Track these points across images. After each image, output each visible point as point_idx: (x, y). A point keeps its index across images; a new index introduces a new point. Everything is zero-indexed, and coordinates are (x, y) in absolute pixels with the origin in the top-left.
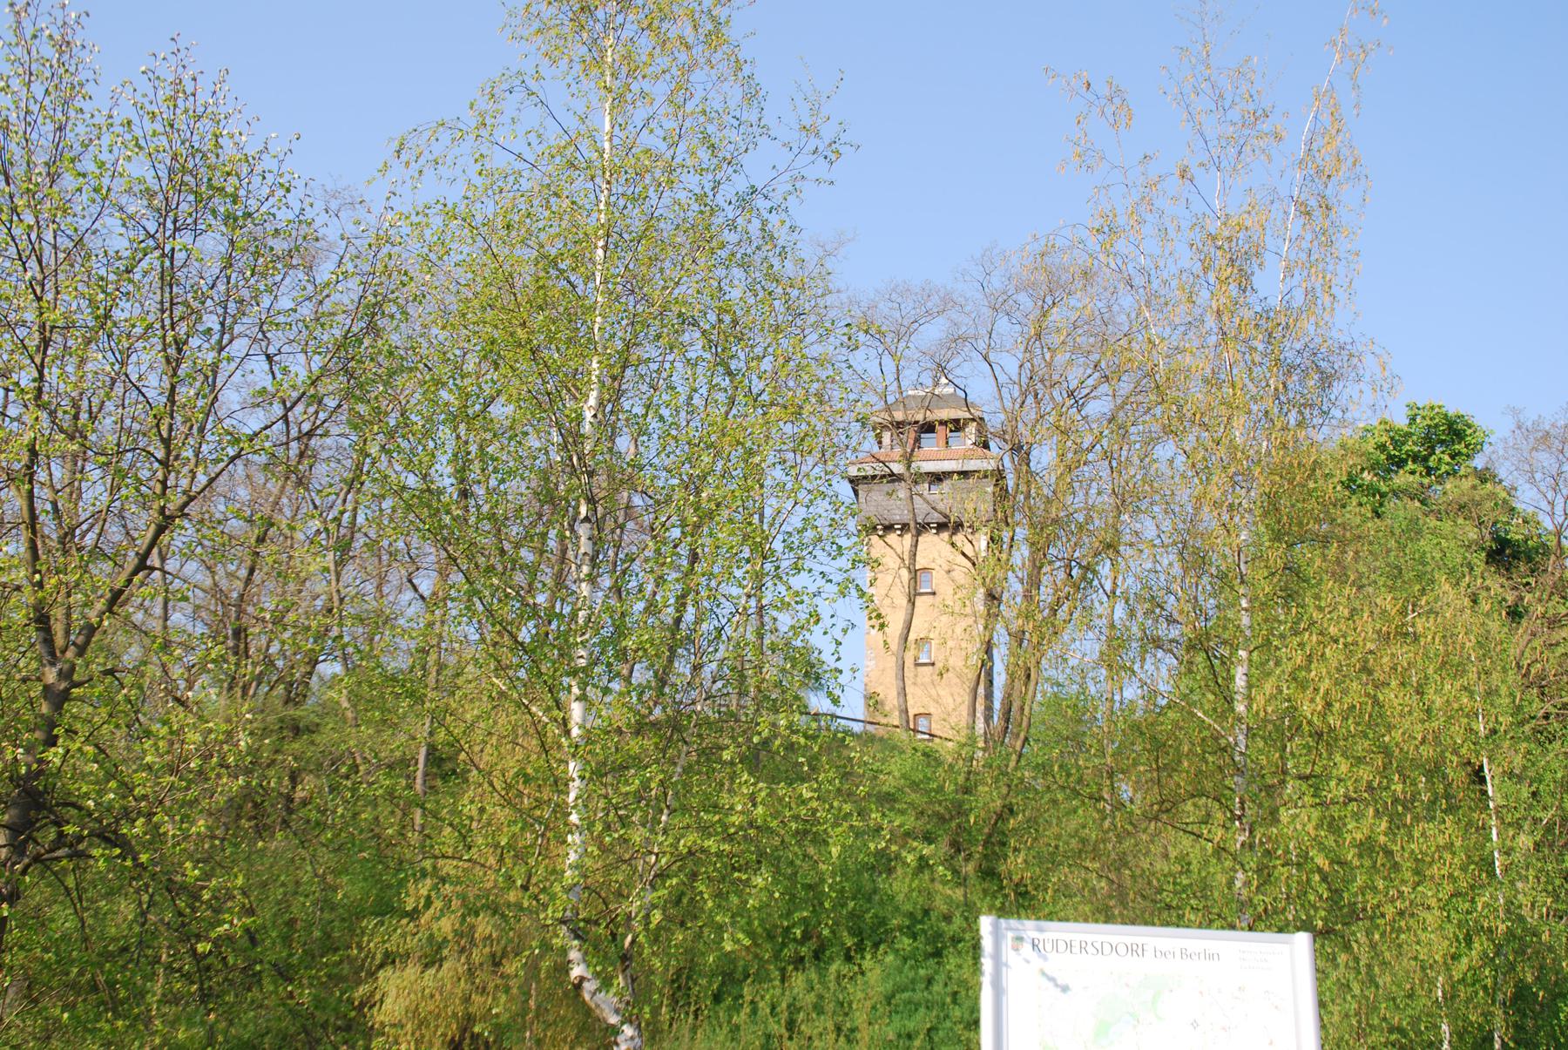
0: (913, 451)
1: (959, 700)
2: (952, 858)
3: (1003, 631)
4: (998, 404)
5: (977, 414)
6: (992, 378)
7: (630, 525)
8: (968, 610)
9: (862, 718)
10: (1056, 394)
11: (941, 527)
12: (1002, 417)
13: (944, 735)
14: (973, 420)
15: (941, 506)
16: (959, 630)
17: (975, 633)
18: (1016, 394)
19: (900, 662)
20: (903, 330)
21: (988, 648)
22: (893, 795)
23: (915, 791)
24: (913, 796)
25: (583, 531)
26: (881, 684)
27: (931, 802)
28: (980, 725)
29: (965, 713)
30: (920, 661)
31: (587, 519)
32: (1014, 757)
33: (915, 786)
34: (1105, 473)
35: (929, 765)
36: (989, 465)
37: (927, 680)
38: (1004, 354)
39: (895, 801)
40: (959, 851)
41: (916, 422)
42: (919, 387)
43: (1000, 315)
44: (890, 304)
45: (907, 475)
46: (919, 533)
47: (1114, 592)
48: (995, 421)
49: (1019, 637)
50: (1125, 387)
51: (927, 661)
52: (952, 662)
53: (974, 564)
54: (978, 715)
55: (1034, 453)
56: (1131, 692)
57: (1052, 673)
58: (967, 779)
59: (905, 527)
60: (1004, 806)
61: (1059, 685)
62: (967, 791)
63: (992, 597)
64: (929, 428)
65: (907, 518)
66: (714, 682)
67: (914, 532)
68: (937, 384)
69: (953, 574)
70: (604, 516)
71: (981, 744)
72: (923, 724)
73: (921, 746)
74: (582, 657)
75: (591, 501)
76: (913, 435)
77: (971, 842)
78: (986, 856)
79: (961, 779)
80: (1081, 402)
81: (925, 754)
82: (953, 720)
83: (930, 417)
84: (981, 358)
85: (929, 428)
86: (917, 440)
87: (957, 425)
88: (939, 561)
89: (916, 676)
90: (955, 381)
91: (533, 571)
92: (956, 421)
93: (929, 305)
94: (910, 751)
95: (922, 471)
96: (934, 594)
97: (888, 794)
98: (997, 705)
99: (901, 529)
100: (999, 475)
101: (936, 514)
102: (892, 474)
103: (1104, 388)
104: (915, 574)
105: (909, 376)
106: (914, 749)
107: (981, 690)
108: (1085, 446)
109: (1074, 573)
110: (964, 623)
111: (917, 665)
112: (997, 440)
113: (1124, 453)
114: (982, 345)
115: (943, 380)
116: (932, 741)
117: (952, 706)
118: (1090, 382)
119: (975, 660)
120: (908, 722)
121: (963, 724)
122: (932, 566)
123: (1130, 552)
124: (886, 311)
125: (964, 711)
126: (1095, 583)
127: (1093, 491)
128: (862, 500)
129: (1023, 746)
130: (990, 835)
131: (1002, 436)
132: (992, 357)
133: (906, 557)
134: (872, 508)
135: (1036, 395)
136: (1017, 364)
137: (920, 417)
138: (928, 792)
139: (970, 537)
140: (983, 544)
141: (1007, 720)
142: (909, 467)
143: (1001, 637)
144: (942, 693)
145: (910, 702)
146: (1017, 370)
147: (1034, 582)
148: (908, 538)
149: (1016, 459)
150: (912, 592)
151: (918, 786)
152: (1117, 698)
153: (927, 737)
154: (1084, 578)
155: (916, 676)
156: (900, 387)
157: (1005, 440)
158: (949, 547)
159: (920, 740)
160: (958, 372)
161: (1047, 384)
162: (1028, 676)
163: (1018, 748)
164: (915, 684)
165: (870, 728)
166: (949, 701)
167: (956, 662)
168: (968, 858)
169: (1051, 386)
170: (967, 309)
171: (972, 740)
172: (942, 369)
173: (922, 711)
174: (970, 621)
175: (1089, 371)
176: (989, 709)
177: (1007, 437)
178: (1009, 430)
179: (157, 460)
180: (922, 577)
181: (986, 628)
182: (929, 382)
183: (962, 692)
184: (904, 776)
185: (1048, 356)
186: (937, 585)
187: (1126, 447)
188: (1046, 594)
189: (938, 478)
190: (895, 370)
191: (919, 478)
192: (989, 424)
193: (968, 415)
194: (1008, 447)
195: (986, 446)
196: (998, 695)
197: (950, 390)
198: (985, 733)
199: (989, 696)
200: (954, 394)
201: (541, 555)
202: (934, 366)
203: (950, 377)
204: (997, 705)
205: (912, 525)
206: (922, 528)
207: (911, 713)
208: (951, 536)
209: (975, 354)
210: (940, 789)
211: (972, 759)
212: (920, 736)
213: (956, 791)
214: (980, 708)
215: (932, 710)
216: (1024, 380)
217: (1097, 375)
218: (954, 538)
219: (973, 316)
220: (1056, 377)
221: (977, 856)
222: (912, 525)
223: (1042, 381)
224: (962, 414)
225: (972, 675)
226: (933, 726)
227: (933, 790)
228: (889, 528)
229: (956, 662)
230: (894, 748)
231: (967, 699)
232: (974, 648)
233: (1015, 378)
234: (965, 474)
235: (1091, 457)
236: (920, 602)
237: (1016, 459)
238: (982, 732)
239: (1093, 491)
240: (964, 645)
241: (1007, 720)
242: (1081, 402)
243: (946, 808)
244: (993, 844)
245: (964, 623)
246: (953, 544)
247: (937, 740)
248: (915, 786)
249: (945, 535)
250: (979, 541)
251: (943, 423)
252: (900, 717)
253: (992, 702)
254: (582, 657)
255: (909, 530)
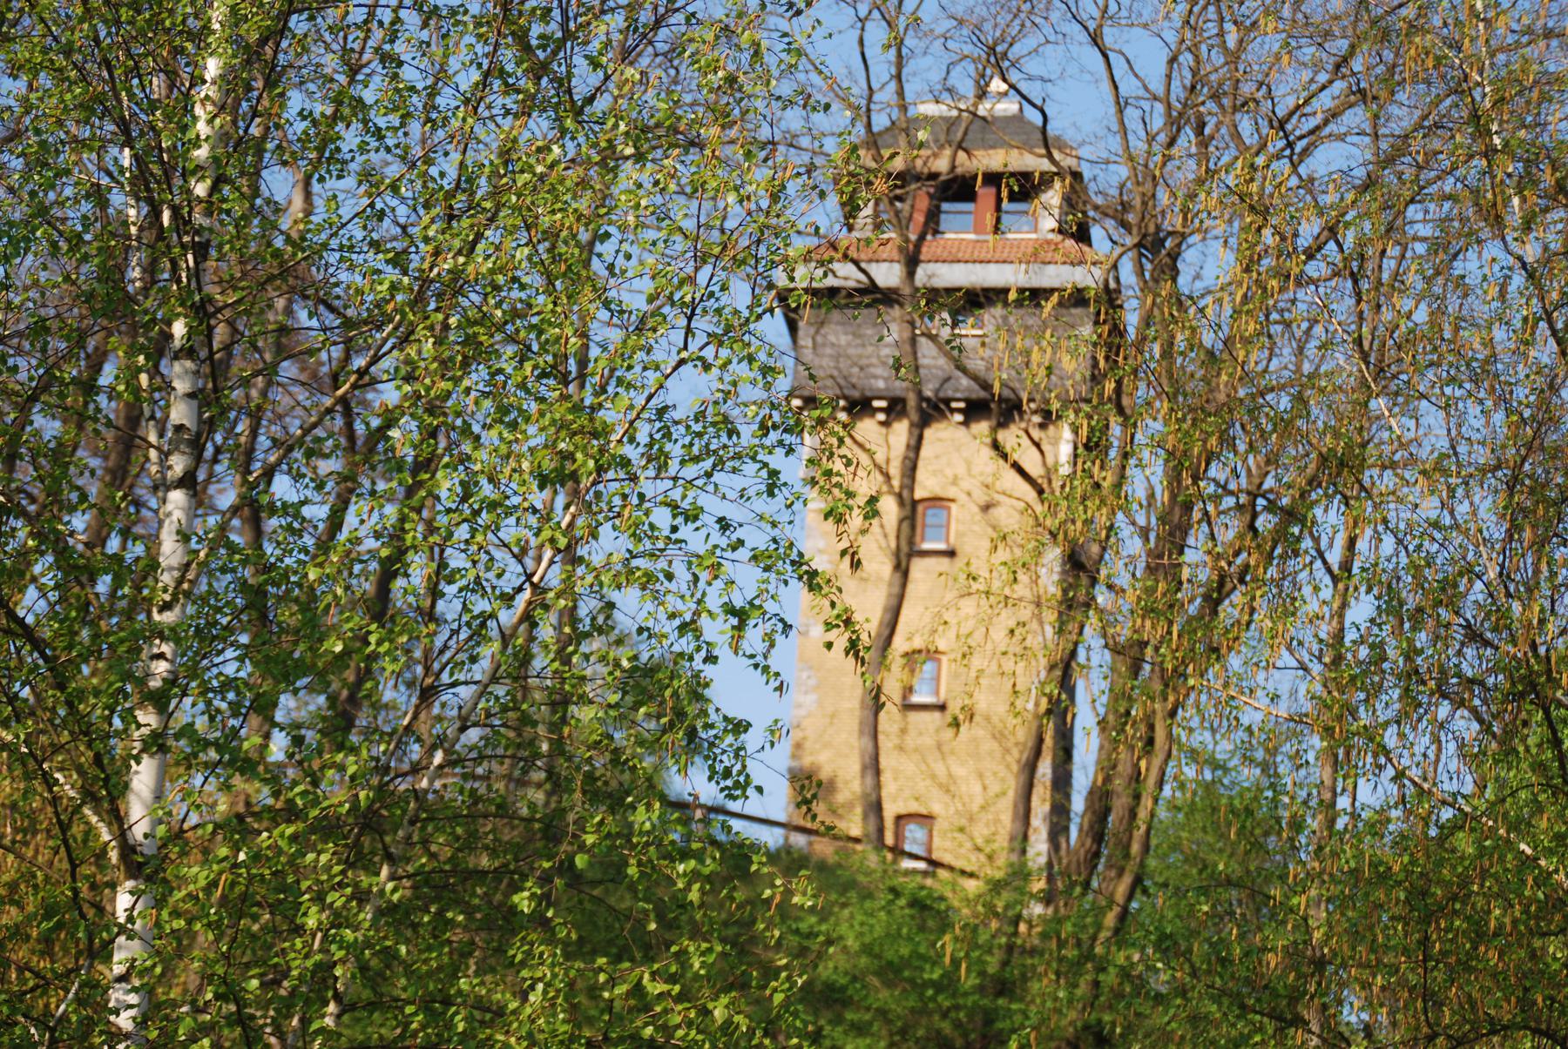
0: (922, 238)
1: (995, 788)
3: (1096, 643)
4: (1115, 143)
5: (1068, 162)
6: (1106, 86)
7: (288, 369)
8: (1022, 590)
9: (782, 818)
10: (1245, 126)
11: (975, 410)
13: (959, 864)
15: (976, 364)
16: (999, 635)
17: (1034, 641)
18: (1157, 122)
19: (894, 602)
21: (1065, 670)
22: (843, 989)
23: (889, 984)
24: (884, 994)
25: (181, 376)
28: (1039, 847)
30: (916, 699)
31: (188, 352)
33: (890, 972)
34: (1344, 306)
35: (922, 928)
36: (1087, 277)
37: (928, 741)
38: (1138, 32)
39: (847, 1003)
41: (933, 176)
42: (945, 96)
46: (924, 421)
47: (1346, 566)
48: (1107, 180)
49: (1130, 655)
50: (1401, 115)
51: (942, 546)
52: (982, 702)
53: (1040, 492)
55: (1190, 258)
56: (1372, 793)
57: (1201, 738)
58: (1005, 964)
59: (896, 408)
60: (1086, 1027)
61: (1216, 765)
62: (1003, 987)
63: (1078, 566)
64: (959, 189)
66: (463, 729)
67: (915, 416)
68: (982, 94)
69: (994, 512)
70: (227, 348)
72: (914, 837)
73: (912, 884)
74: (161, 656)
75: (202, 312)
76: (923, 203)
79: (993, 964)
80: (1299, 147)
81: (915, 903)
82: (980, 832)
84: (1084, 37)
85: (959, 189)
86: (933, 217)
87: (1026, 188)
88: (966, 484)
89: (903, 731)
90: (1023, 87)
91: (61, 454)
92: (1025, 176)
94: (883, 897)
96: (951, 554)
97: (830, 987)
98: (1078, 804)
99: (886, 411)
100: (1111, 297)
101: (965, 382)
102: (872, 288)
103: (1356, 117)
104: (911, 509)
105: (925, 70)
107: (1045, 768)
108: (1304, 242)
109: (1260, 523)
110: (1007, 619)
111: (909, 707)
112: (1110, 223)
113: (1389, 265)
115: (997, 85)
116: (934, 875)
118: (1325, 101)
119: (1032, 704)
120: (881, 830)
121: (1002, 842)
122: (951, 492)
123: (1388, 480)
125: (1005, 814)
126: (1307, 543)
128: (805, 341)
129: (1130, 897)
131: (1119, 213)
132: (1110, 36)
133: (895, 470)
134: (826, 362)
135: (1200, 127)
136: (1164, 55)
137: (941, 165)
139: (1036, 434)
140: (1065, 450)
142: (911, 274)
143: (1095, 656)
144: (959, 771)
146: (1162, 68)
147: (1174, 532)
148: (901, 429)
150: (905, 548)
152: (1343, 802)
153: (922, 865)
154: (1280, 534)
155: (903, 731)
156: (901, 93)
157: (1124, 225)
158: (987, 452)
159: (908, 873)
161: (1226, 101)
162: (1150, 742)
164: (901, 748)
165: (799, 840)
166: (972, 790)
167: (990, 701)
169: (1235, 109)
171: (1020, 874)
172: (996, 59)
173: (914, 807)
174: (1026, 613)
175: (1323, 78)
176: (1060, 811)
177: (1131, 218)
178: (1137, 202)
179: (869, 125)
180: (930, 517)
181: (1060, 632)
182: (967, 88)
183: (1003, 772)
184: (867, 949)
185: (1232, 40)
186: (959, 535)
187: (1394, 251)
188: (1195, 557)
189: (975, 300)
191: (935, 297)
192: (1092, 187)
193: (1045, 165)
194: (1130, 241)
195: (1082, 236)
196: (1083, 777)
197: (1009, 107)
198: (1050, 865)
199: (1062, 781)
200: (1019, 117)
201: (80, 427)
202: (978, 52)
203: (1014, 76)
204: (1078, 804)
206: (932, 410)
208: (994, 430)
210: (948, 984)
211: (1018, 919)
212: (907, 864)
213: (981, 989)
214: (1041, 806)
215: (936, 808)
216: (1177, 90)
217: (1339, 86)
218: (1002, 436)
220: (1247, 89)
223: (1215, 96)
224: (1035, 163)
225: (1023, 734)
226: (937, 842)
227: (932, 983)
228: (860, 406)
229: (990, 701)
230: (850, 885)
231: (1011, 786)
232: (1033, 676)
233: (1157, 87)
234: (1035, 296)
235: (1314, 269)
236: (920, 569)
238: (1043, 860)
240: (1008, 665)
242: (1299, 147)
243: (958, 1025)
245: (1007, 619)
246: (996, 446)
247: (943, 874)
248: (890, 972)
249: (982, 427)
250: (1056, 442)
251: (993, 179)
252: (865, 817)
253: (1068, 797)
254: (161, 656)
255: (903, 413)
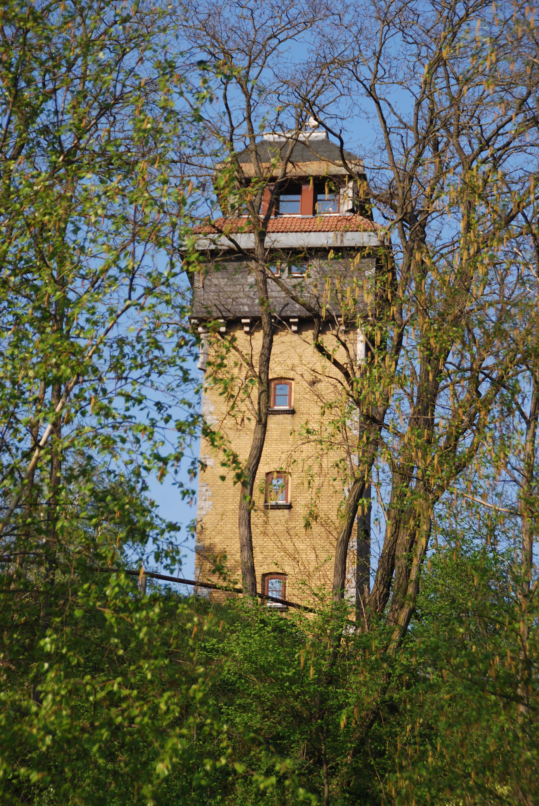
0: (267, 218)
1: (323, 556)
2: (311, 772)
6: (378, 121)
9: (192, 578)
10: (463, 141)
12: (390, 174)
13: (304, 604)
14: (351, 178)
19: (258, 443)
20: (256, 49)
22: (234, 683)
26: (220, 533)
27: (282, 696)
28: (351, 592)
29: (331, 574)
32: (396, 636)
39: (235, 692)
40: (319, 763)
41: (273, 179)
43: (393, 31)
44: (239, 11)
45: (259, 252)
46: (273, 331)
53: (347, 375)
54: (349, 576)
55: (433, 225)
58: (332, 665)
65: (258, 310)
68: (301, 126)
69: (319, 386)
71: (352, 618)
77: (338, 751)
78: (355, 771)
79: (325, 665)
82: (315, 583)
83: (293, 171)
84: (363, 90)
86: (275, 204)
88: (300, 370)
90: (329, 123)
93: (293, 12)
95: (277, 245)
98: (374, 564)
106: (262, 621)
107: (353, 543)
114: (365, 72)
115: (312, 122)
117: (313, 564)
120: (254, 584)
122: (291, 375)
124: (233, 21)
127: (511, 279)
130: (362, 742)
132: (379, 90)
138: (280, 681)
139: (343, 338)
140: (360, 348)
141: (388, 585)
142: (262, 241)
144: (301, 546)
145: (258, 557)
146: (412, 111)
148: (259, 337)
149: (408, 232)
150: (264, 410)
151: (267, 672)
156: (251, 130)
157: (393, 207)
159: (271, 609)
160: (331, 109)
163: (402, 622)
164: (265, 534)
165: (205, 591)
168: (331, 774)
170: (347, 19)
173: (274, 569)
177: (396, 202)
178: (400, 192)
180: (279, 389)
182: (291, 123)
184: (248, 658)
190: (244, 105)
197: (321, 135)
198: (358, 602)
203: (321, 116)
204: (374, 564)
205: (265, 320)
207: (259, 571)
208: (316, 337)
209: (354, 84)
210: (301, 676)
214: (351, 567)
215: (287, 569)
216: (422, 124)
219: (328, 82)
221: (345, 770)
222: (265, 320)
225: (341, 524)
226: (288, 590)
227: (289, 679)
233: (409, 120)
237: (408, 232)
239: (511, 279)
241: (388, 585)
243: (305, 703)
244: (366, 754)
245: (336, 455)
246: (320, 348)
249: (309, 334)
250: (354, 343)
